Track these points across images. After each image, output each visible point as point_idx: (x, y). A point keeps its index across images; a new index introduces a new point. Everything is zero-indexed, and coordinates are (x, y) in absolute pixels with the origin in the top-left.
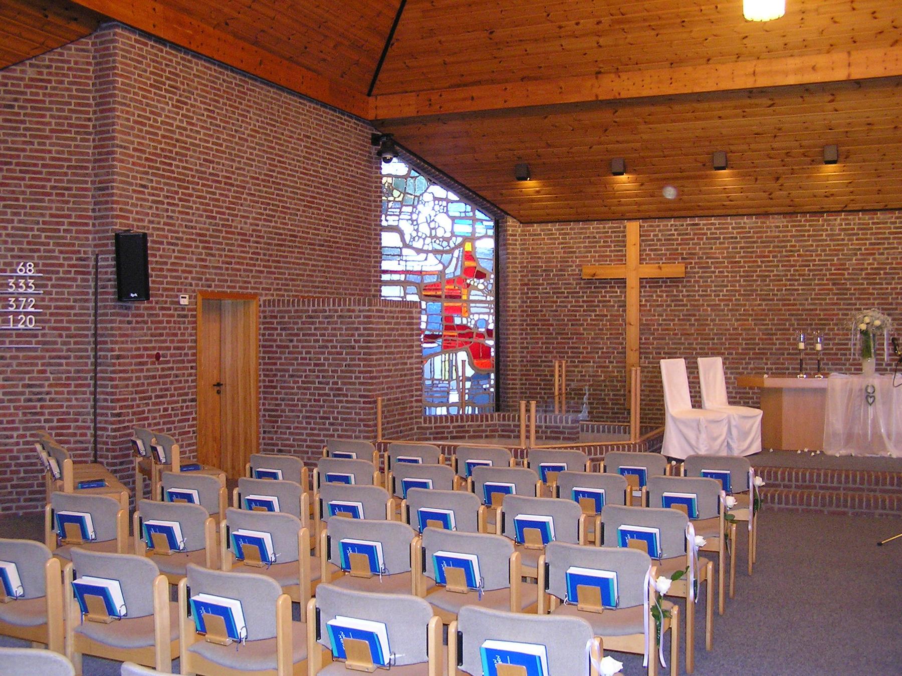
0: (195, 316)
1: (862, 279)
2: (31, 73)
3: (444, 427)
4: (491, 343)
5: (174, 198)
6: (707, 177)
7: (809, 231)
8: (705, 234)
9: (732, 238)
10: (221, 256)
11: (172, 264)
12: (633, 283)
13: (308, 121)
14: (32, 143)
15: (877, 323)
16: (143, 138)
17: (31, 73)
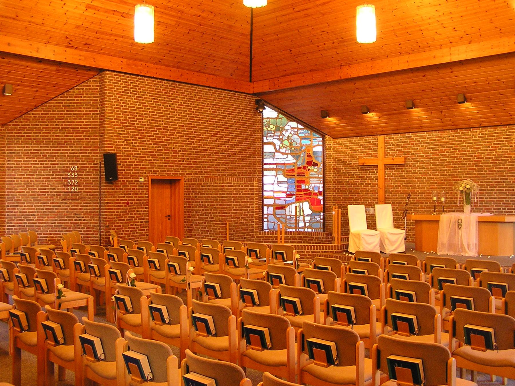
0: (148, 186)
1: (491, 163)
2: (76, 92)
3: (269, 237)
4: (321, 198)
5: (136, 138)
6: (408, 113)
7: (464, 138)
8: (415, 141)
9: (427, 143)
10: (162, 161)
11: (135, 165)
12: (381, 167)
13: (214, 97)
14: (77, 119)
15: (468, 187)
16: (119, 114)
17: (76, 92)
